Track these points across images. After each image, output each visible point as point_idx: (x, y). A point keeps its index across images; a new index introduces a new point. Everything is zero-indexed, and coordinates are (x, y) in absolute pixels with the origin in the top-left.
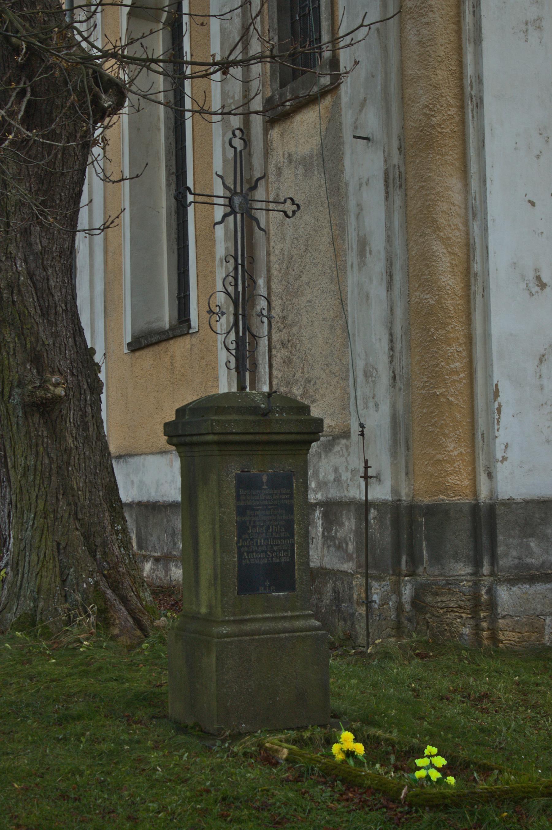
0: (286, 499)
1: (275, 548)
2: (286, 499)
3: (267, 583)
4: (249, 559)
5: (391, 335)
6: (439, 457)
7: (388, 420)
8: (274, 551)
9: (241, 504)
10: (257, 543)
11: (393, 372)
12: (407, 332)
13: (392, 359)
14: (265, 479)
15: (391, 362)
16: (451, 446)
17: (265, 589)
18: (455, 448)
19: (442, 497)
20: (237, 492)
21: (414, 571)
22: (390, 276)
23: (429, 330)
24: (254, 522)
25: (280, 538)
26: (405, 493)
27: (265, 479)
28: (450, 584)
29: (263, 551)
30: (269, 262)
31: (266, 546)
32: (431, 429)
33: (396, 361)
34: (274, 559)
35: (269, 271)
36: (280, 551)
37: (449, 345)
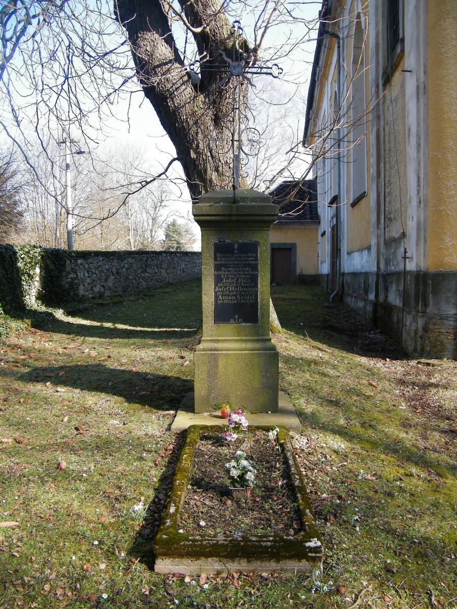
0: (252, 260)
1: (243, 293)
2: (252, 260)
3: (236, 317)
4: (223, 300)
5: (419, 178)
6: (441, 246)
7: (416, 225)
8: (242, 295)
9: (218, 263)
10: (229, 289)
11: (420, 199)
12: (426, 175)
13: (418, 191)
14: (236, 246)
15: (418, 193)
16: (448, 240)
17: (235, 320)
18: (450, 241)
19: (441, 269)
20: (215, 255)
21: (426, 311)
22: (419, 145)
23: (437, 173)
24: (228, 275)
25: (247, 287)
26: (423, 266)
27: (236, 246)
28: (443, 318)
29: (233, 295)
30: (385, 155)
31: (236, 292)
32: (437, 230)
33: (421, 194)
34: (242, 301)
35: (385, 159)
36: (247, 295)
37: (449, 181)
